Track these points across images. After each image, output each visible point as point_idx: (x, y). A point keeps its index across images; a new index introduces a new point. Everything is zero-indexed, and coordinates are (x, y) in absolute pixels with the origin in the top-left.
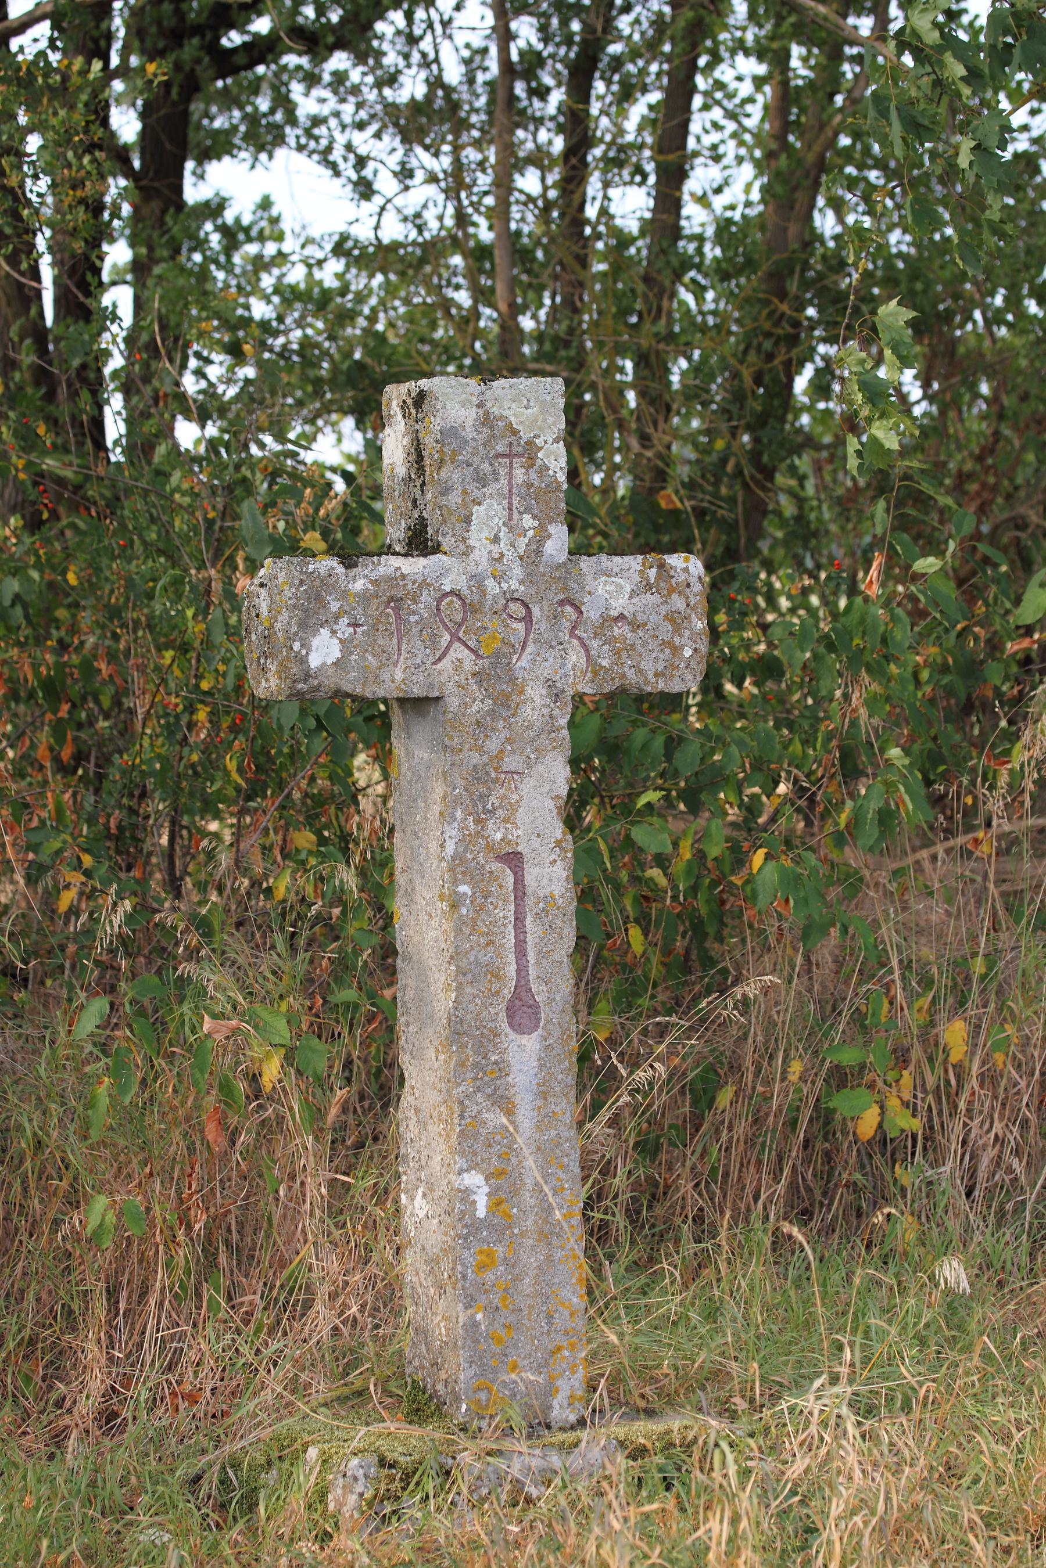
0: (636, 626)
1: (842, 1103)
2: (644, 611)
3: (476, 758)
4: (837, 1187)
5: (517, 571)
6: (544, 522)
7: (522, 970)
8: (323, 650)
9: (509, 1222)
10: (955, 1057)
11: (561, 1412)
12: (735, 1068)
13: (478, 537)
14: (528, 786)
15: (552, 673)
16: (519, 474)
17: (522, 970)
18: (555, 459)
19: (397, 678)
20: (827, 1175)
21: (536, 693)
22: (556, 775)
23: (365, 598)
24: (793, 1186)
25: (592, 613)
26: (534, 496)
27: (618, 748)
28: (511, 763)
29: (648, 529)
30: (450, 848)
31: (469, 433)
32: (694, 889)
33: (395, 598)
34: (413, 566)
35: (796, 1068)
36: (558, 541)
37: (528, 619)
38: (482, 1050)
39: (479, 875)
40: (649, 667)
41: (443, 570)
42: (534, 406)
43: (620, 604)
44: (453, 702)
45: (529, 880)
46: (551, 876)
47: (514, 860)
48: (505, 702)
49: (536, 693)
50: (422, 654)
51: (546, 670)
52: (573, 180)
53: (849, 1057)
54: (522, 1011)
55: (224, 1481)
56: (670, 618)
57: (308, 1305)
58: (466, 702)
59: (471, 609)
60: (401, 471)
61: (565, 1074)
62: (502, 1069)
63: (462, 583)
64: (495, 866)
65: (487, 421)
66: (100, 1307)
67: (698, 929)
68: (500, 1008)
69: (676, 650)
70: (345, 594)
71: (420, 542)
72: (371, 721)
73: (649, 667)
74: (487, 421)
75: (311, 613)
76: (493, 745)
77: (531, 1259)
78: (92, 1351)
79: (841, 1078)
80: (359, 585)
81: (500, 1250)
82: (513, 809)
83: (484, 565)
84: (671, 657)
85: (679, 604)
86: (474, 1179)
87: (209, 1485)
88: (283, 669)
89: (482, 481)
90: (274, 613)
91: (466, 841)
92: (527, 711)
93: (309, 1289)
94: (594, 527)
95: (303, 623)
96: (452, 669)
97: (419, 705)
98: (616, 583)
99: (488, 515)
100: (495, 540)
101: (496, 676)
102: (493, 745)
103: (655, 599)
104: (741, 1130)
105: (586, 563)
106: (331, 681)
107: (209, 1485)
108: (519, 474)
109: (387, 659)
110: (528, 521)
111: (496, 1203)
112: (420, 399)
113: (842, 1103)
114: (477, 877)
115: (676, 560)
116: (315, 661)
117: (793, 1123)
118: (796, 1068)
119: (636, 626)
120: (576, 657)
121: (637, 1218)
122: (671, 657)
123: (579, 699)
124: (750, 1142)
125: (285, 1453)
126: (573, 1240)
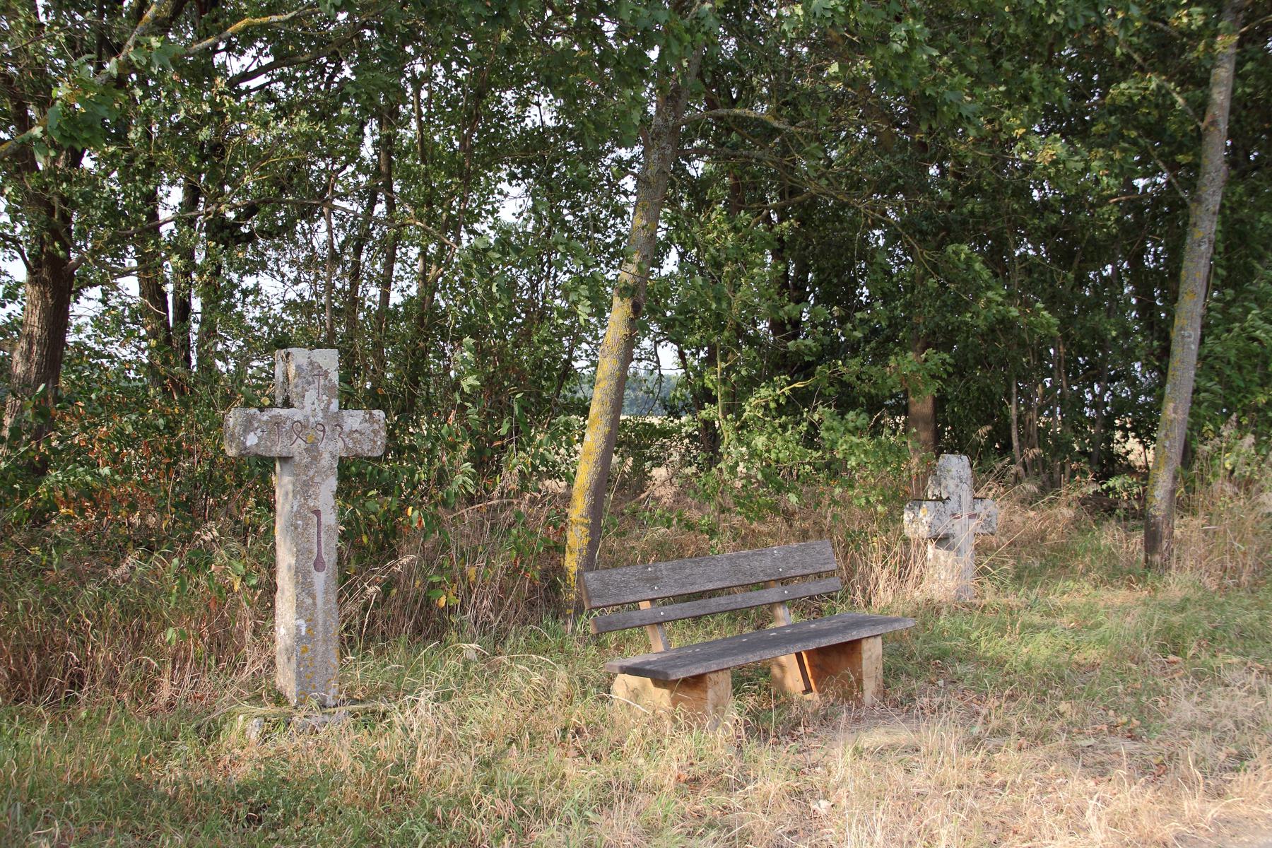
0: (361, 434)
1: (432, 594)
2: (364, 429)
3: (305, 478)
4: (430, 625)
5: (321, 414)
6: (330, 398)
7: (319, 550)
8: (252, 440)
9: (313, 637)
10: (473, 579)
11: (330, 702)
12: (398, 582)
13: (307, 402)
14: (323, 487)
15: (332, 449)
16: (322, 382)
17: (319, 550)
18: (335, 377)
19: (277, 450)
20: (427, 619)
21: (326, 456)
22: (332, 483)
23: (267, 422)
24: (415, 622)
25: (346, 429)
26: (329, 389)
27: (353, 476)
28: (317, 479)
29: (374, 400)
30: (295, 509)
31: (305, 367)
32: (386, 521)
33: (277, 423)
34: (284, 412)
35: (418, 583)
36: (335, 404)
37: (324, 431)
38: (304, 577)
39: (304, 519)
40: (366, 448)
41: (295, 414)
42: (329, 359)
43: (356, 426)
44: (297, 459)
45: (323, 519)
46: (330, 519)
47: (317, 513)
48: (315, 459)
49: (326, 456)
50: (287, 442)
51: (330, 448)
52: (354, 285)
53: (436, 579)
54: (319, 564)
55: (209, 729)
56: (373, 431)
57: (244, 665)
58: (302, 458)
59: (304, 427)
60: (281, 379)
61: (334, 588)
62: (312, 584)
63: (301, 418)
64: (311, 515)
65: (311, 363)
66: (169, 667)
67: (386, 536)
68: (311, 564)
69: (375, 442)
70: (260, 421)
71: (287, 404)
72: (266, 464)
73: (366, 448)
74: (311, 363)
75: (248, 426)
76: (311, 473)
77: (320, 649)
78: (166, 681)
79: (433, 586)
80: (265, 418)
81: (310, 646)
82: (317, 495)
83: (309, 412)
84: (374, 445)
85: (376, 426)
86: (301, 622)
87: (204, 730)
88: (237, 446)
89: (309, 383)
90: (235, 427)
91: (301, 506)
92: (323, 462)
93: (245, 660)
94: (348, 400)
95: (244, 432)
96: (297, 447)
97: (285, 460)
98: (354, 419)
99: (311, 395)
100: (313, 404)
101: (313, 450)
102: (311, 473)
103: (367, 425)
104: (399, 603)
105: (345, 412)
106: (254, 450)
107: (204, 730)
108: (322, 382)
109: (274, 443)
110: (325, 397)
111: (309, 630)
112: (288, 355)
113: (432, 594)
114: (304, 518)
115: (375, 412)
116: (248, 444)
117: (416, 602)
118: (418, 583)
119: (361, 434)
120: (340, 444)
121: (361, 635)
122: (374, 445)
123: (341, 458)
124: (402, 607)
125: (230, 716)
126: (334, 646)
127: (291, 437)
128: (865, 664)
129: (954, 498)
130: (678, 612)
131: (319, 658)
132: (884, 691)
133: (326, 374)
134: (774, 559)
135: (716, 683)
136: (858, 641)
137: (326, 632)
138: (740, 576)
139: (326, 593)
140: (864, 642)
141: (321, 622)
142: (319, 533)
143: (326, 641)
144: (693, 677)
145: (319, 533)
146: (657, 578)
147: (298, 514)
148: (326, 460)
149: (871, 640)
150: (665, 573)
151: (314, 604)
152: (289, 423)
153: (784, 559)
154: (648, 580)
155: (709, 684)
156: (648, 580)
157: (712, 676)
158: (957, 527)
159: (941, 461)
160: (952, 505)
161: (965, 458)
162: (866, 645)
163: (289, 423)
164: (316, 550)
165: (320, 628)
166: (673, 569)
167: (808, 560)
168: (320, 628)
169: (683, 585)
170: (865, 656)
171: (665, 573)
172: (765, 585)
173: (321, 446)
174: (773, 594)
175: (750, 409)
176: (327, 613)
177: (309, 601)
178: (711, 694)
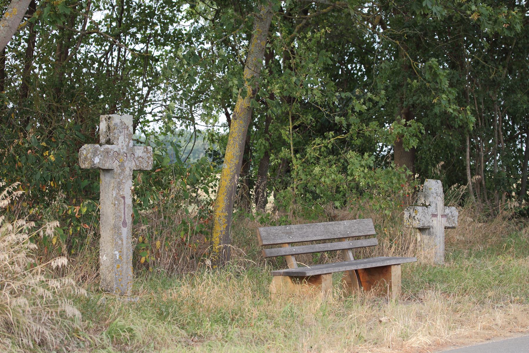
0: (143, 158)
3: (119, 180)
5: (125, 148)
7: (125, 217)
14: (126, 185)
15: (130, 165)
16: (126, 131)
17: (125, 217)
23: (103, 152)
25: (136, 156)
28: (124, 181)
31: (119, 124)
33: (107, 152)
37: (127, 156)
40: (145, 166)
43: (140, 155)
44: (115, 170)
47: (124, 198)
48: (123, 171)
51: (129, 165)
54: (125, 224)
56: (148, 157)
62: (121, 234)
64: (121, 199)
65: (121, 122)
69: (148, 163)
71: (108, 142)
73: (145, 166)
74: (121, 122)
77: (125, 267)
80: (102, 149)
81: (120, 265)
82: (124, 189)
85: (149, 155)
89: (120, 132)
92: (126, 172)
96: (114, 165)
97: (108, 171)
99: (121, 138)
102: (121, 178)
103: (145, 154)
106: (97, 166)
108: (126, 131)
109: (106, 162)
110: (127, 140)
112: (109, 118)
114: (118, 200)
116: (95, 162)
119: (143, 158)
120: (134, 163)
123: (134, 170)
127: (113, 159)
128: (393, 278)
129: (433, 205)
130: (301, 250)
131: (124, 271)
132: (403, 290)
133: (128, 128)
134: (345, 227)
135: (326, 280)
136: (390, 266)
137: (128, 258)
138: (329, 234)
139: (127, 239)
140: (392, 267)
141: (125, 253)
142: (124, 208)
143: (127, 263)
144: (315, 275)
145: (124, 208)
146: (291, 233)
147: (116, 198)
148: (128, 172)
149: (396, 266)
150: (294, 230)
151: (122, 244)
152: (112, 152)
153: (350, 227)
154: (287, 233)
155: (323, 280)
156: (287, 233)
157: (324, 276)
158: (435, 222)
159: (426, 183)
160: (432, 209)
161: (439, 181)
162: (393, 269)
163: (112, 152)
164: (123, 217)
165: (125, 256)
166: (298, 229)
167: (361, 228)
168: (125, 256)
169: (303, 237)
170: (393, 274)
171: (294, 230)
172: (340, 239)
173: (126, 164)
174: (345, 245)
175: (311, 151)
176: (128, 248)
177: (120, 242)
178: (323, 285)
